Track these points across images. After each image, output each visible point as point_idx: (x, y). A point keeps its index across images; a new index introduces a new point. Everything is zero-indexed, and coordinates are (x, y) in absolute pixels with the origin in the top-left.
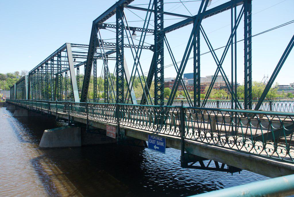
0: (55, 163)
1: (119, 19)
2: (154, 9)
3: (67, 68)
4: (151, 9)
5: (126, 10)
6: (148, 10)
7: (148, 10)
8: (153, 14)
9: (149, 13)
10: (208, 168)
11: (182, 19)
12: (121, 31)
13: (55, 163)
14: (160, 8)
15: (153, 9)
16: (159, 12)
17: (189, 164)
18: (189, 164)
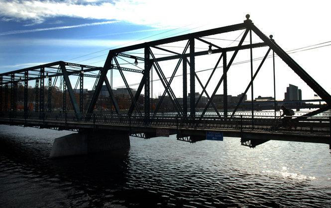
10: (185, 141)
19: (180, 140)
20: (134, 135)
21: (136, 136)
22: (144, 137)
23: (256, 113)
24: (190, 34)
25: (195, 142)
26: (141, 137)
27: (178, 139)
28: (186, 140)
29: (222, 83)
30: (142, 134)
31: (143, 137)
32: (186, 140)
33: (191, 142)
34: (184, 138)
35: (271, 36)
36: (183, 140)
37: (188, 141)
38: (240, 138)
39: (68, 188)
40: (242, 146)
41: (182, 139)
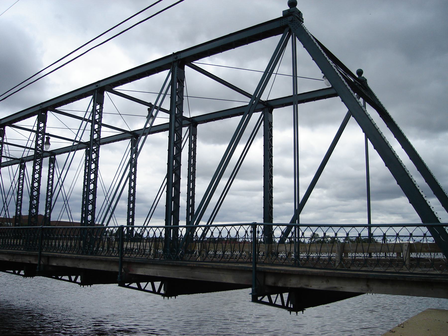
0: (363, 83)
1: (41, 123)
2: (91, 119)
3: (75, 144)
4: (88, 118)
5: (50, 115)
6: (83, 119)
7: (83, 119)
8: (90, 124)
9: (85, 122)
10: (144, 290)
11: (70, 144)
12: (42, 136)
13: (363, 83)
14: (98, 121)
15: (90, 119)
16: (40, 133)
17: (126, 284)
18: (126, 284)
19: (261, 302)
20: (134, 285)
21: (139, 288)
22: (162, 291)
23: (358, 255)
24: (275, 35)
25: (302, 309)
26: (154, 292)
27: (254, 300)
28: (279, 302)
29: (302, 195)
30: (157, 284)
31: (159, 293)
32: (279, 302)
33: (290, 310)
34: (273, 297)
35: (360, 72)
36: (270, 303)
37: (283, 307)
38: (154, 282)
39: (18, 331)
40: (254, 304)
41: (266, 299)
